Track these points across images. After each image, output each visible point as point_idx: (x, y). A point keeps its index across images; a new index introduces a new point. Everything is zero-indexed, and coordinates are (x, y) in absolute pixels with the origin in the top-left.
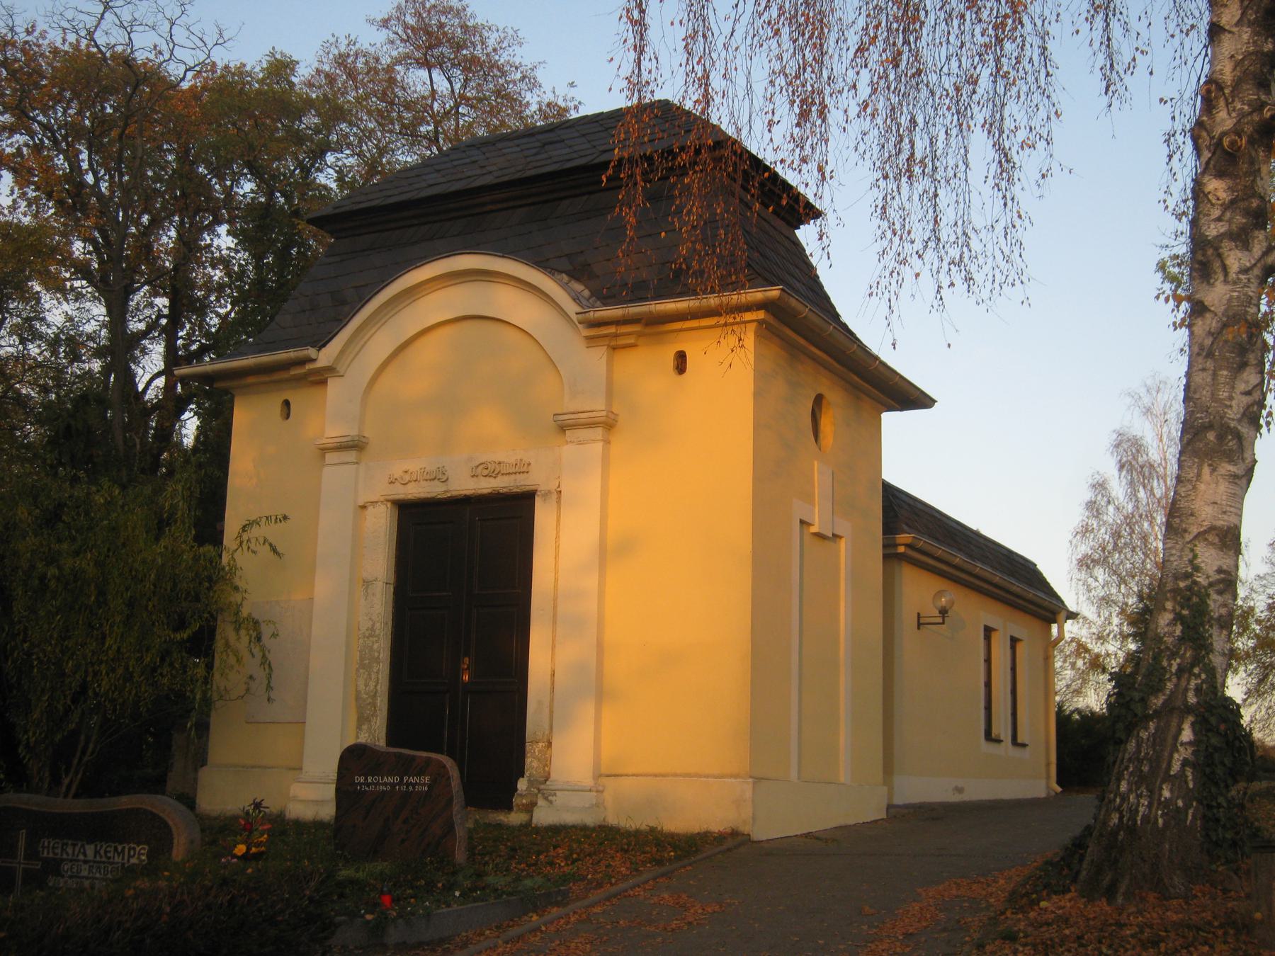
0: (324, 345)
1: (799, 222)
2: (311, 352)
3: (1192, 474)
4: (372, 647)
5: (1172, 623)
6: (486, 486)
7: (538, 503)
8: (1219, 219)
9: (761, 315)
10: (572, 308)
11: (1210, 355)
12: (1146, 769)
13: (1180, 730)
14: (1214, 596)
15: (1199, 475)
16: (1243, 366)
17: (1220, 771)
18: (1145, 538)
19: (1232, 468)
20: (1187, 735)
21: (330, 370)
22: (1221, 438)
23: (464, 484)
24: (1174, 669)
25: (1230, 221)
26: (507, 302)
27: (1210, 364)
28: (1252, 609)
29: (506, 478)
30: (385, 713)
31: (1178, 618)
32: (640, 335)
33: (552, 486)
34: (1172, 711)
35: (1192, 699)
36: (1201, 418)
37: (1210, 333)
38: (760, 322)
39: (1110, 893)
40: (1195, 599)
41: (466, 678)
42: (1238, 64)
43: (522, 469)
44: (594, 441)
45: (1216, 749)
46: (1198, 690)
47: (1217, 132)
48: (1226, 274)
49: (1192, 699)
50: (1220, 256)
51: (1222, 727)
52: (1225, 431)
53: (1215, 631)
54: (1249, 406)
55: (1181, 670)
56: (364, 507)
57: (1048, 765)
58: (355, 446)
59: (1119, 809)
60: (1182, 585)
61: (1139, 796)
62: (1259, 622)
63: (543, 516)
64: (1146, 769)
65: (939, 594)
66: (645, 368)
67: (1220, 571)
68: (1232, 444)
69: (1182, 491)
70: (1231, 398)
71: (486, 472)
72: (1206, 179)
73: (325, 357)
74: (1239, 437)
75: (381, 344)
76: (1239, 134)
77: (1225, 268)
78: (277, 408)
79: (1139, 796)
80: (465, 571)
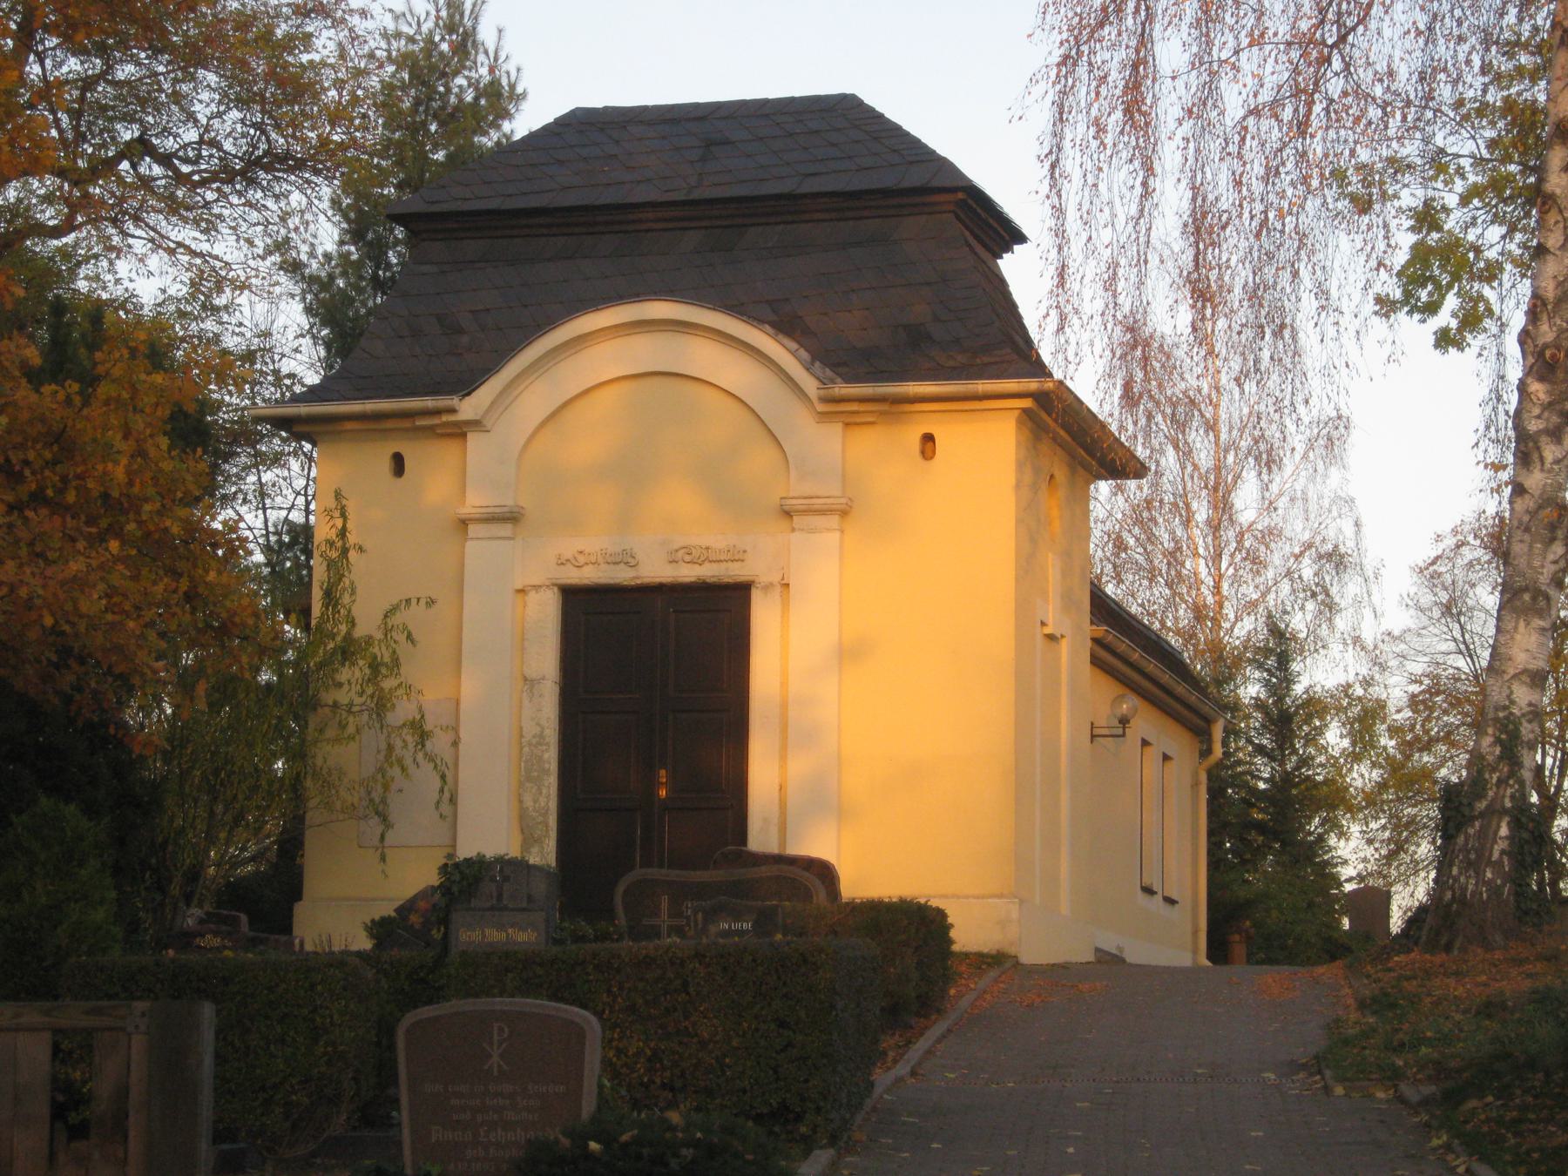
0: (469, 394)
1: (1008, 248)
2: (454, 401)
3: (1510, 626)
4: (541, 758)
5: (1494, 744)
6: (688, 573)
7: (757, 597)
8: (1539, 417)
9: (1027, 403)
10: (810, 384)
11: (1527, 530)
12: (1473, 856)
13: (1499, 827)
14: (1525, 724)
15: (1516, 628)
16: (1553, 540)
17: (1529, 859)
18: (1174, 556)
19: (1542, 623)
20: (1504, 831)
21: (476, 424)
22: (1534, 599)
23: (655, 569)
24: (1494, 780)
25: (1548, 420)
26: (703, 357)
27: (1527, 537)
28: (1381, 705)
29: (715, 566)
30: (553, 834)
31: (1498, 741)
32: (881, 413)
33: (776, 578)
34: (1493, 813)
35: (1508, 804)
36: (1519, 582)
37: (1528, 511)
38: (1025, 411)
39: (1448, 948)
40: (1511, 727)
41: (663, 793)
42: (1559, 284)
43: (737, 556)
44: (828, 530)
45: (1527, 842)
46: (1512, 797)
47: (1540, 341)
48: (1543, 464)
49: (1508, 804)
50: (1538, 448)
51: (1531, 825)
52: (1538, 593)
53: (1525, 752)
54: (1556, 572)
55: (1500, 781)
56: (522, 591)
57: (1195, 932)
58: (511, 517)
59: (1452, 888)
60: (1501, 715)
61: (1468, 878)
62: (1394, 731)
63: (764, 619)
64: (1473, 856)
65: (1118, 699)
66: (877, 454)
67: (1530, 704)
68: (1543, 604)
69: (1502, 639)
70: (1543, 566)
71: (688, 558)
72: (1529, 380)
73: (468, 408)
74: (1548, 598)
75: (535, 401)
76: (1558, 348)
77: (1542, 459)
78: (386, 465)
79: (1468, 878)
80: (657, 673)
